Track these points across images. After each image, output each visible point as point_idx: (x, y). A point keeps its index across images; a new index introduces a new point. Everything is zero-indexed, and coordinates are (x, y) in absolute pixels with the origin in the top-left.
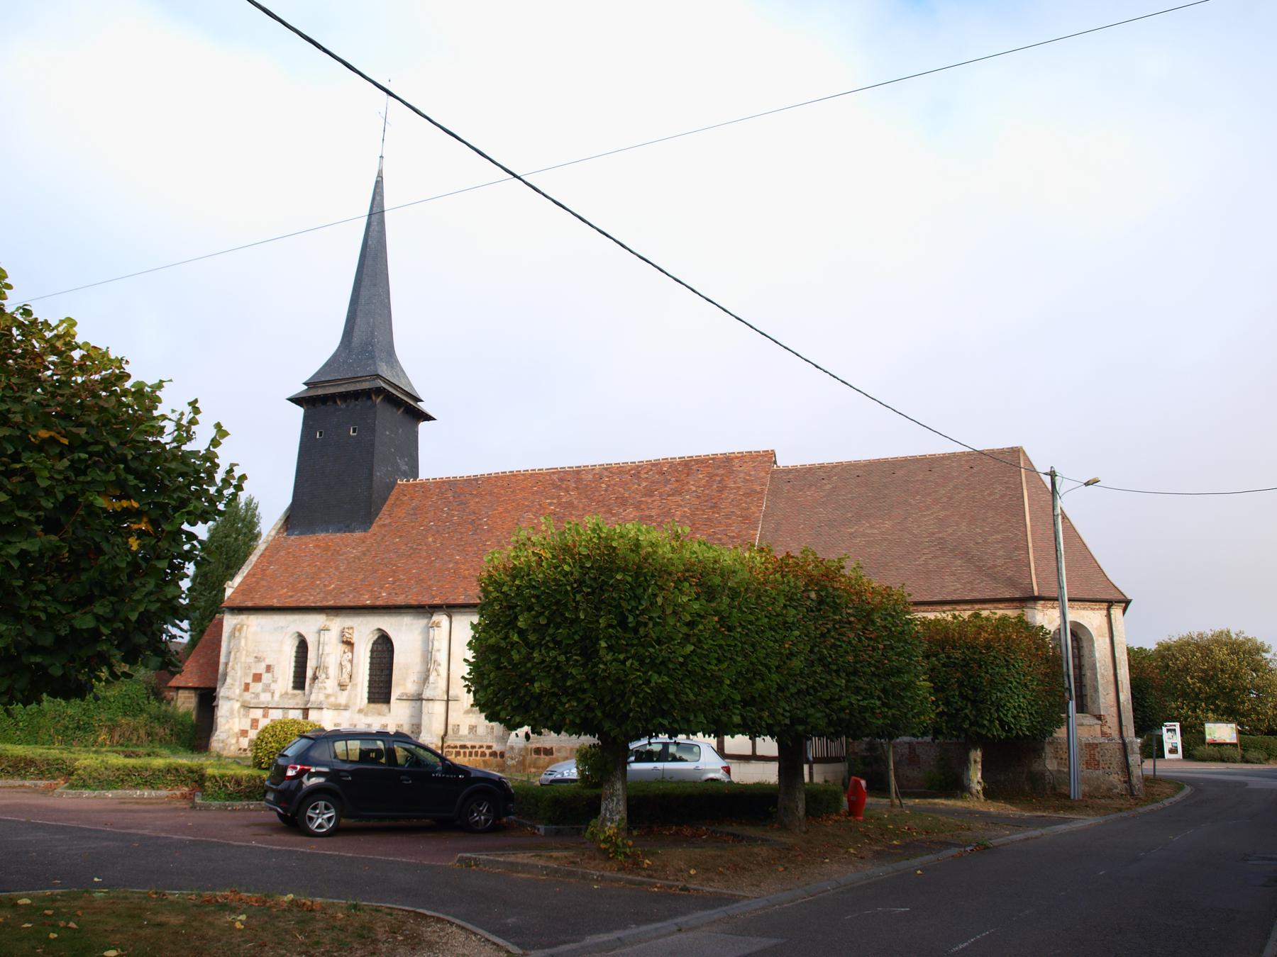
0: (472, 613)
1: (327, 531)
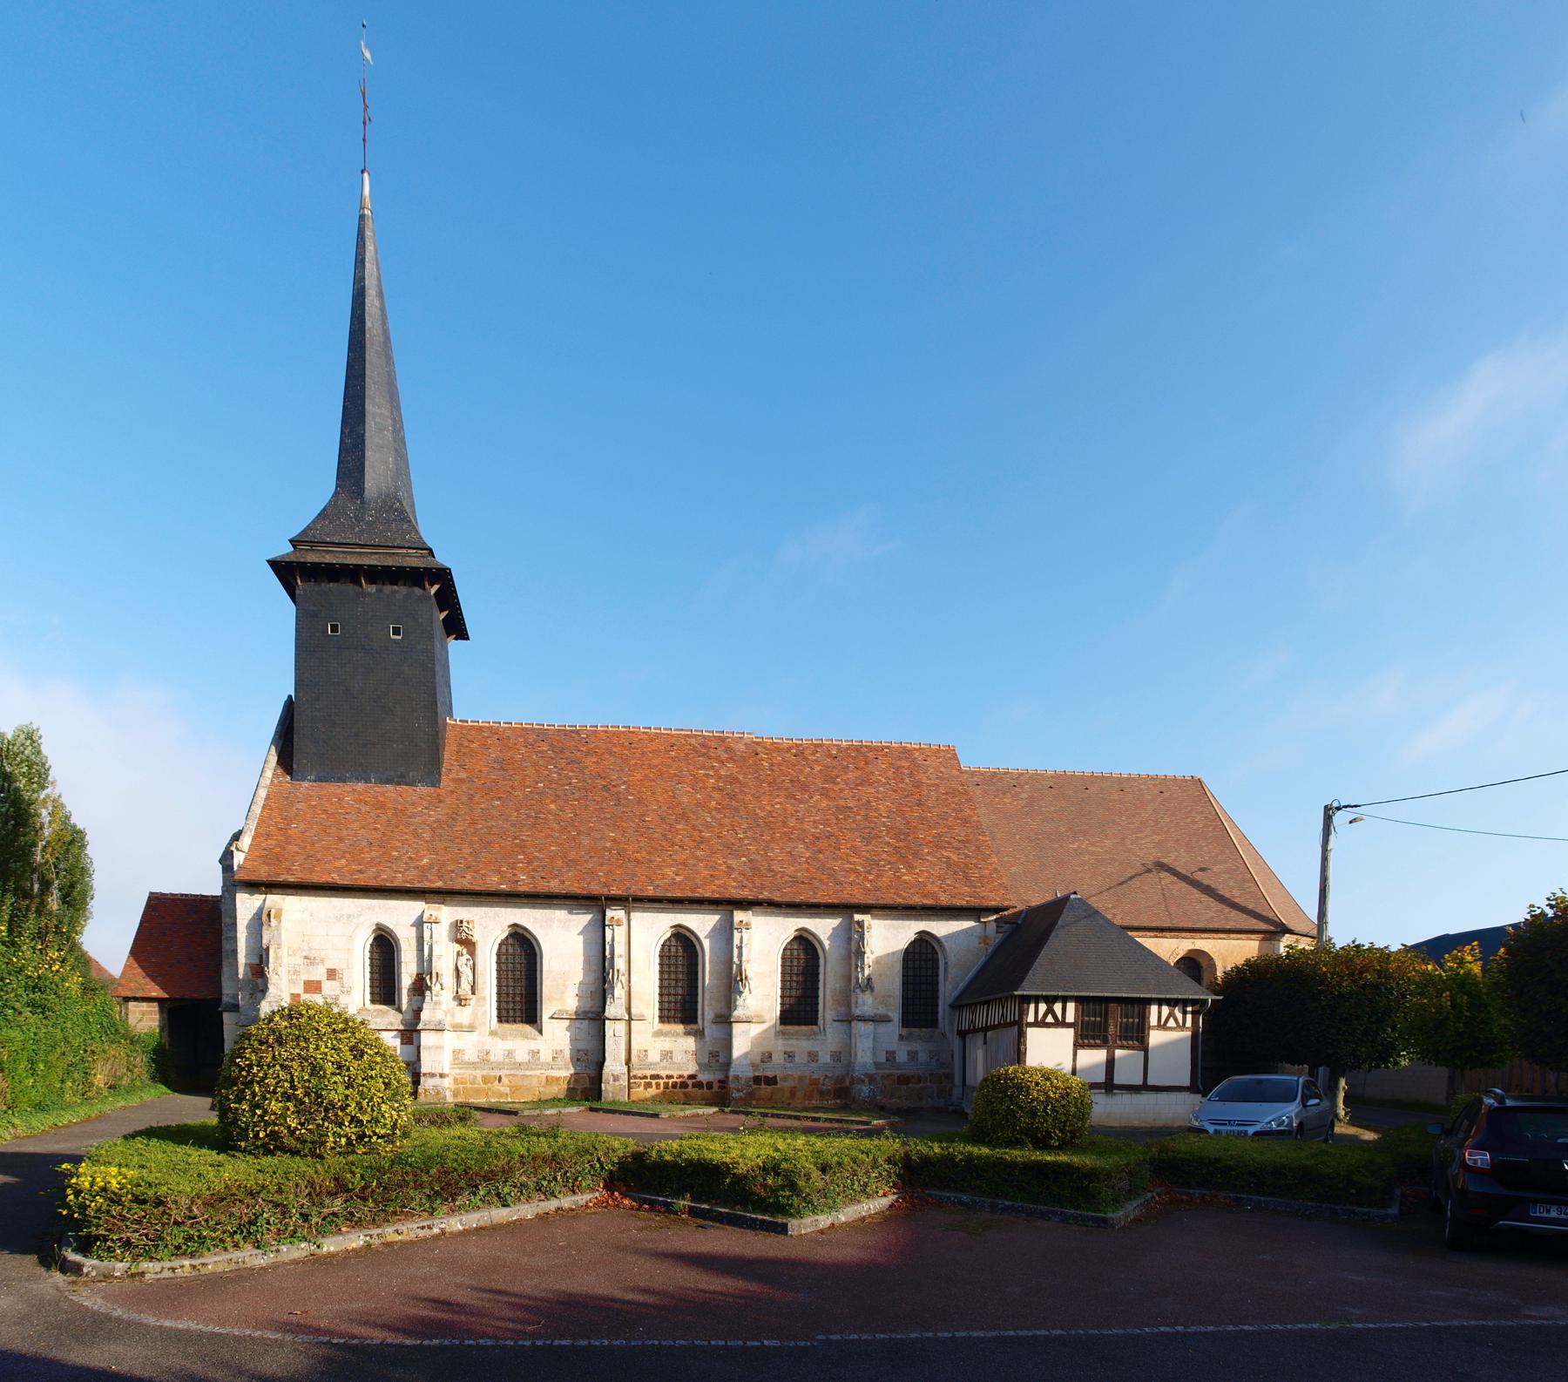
0: (713, 912)
1: (367, 780)
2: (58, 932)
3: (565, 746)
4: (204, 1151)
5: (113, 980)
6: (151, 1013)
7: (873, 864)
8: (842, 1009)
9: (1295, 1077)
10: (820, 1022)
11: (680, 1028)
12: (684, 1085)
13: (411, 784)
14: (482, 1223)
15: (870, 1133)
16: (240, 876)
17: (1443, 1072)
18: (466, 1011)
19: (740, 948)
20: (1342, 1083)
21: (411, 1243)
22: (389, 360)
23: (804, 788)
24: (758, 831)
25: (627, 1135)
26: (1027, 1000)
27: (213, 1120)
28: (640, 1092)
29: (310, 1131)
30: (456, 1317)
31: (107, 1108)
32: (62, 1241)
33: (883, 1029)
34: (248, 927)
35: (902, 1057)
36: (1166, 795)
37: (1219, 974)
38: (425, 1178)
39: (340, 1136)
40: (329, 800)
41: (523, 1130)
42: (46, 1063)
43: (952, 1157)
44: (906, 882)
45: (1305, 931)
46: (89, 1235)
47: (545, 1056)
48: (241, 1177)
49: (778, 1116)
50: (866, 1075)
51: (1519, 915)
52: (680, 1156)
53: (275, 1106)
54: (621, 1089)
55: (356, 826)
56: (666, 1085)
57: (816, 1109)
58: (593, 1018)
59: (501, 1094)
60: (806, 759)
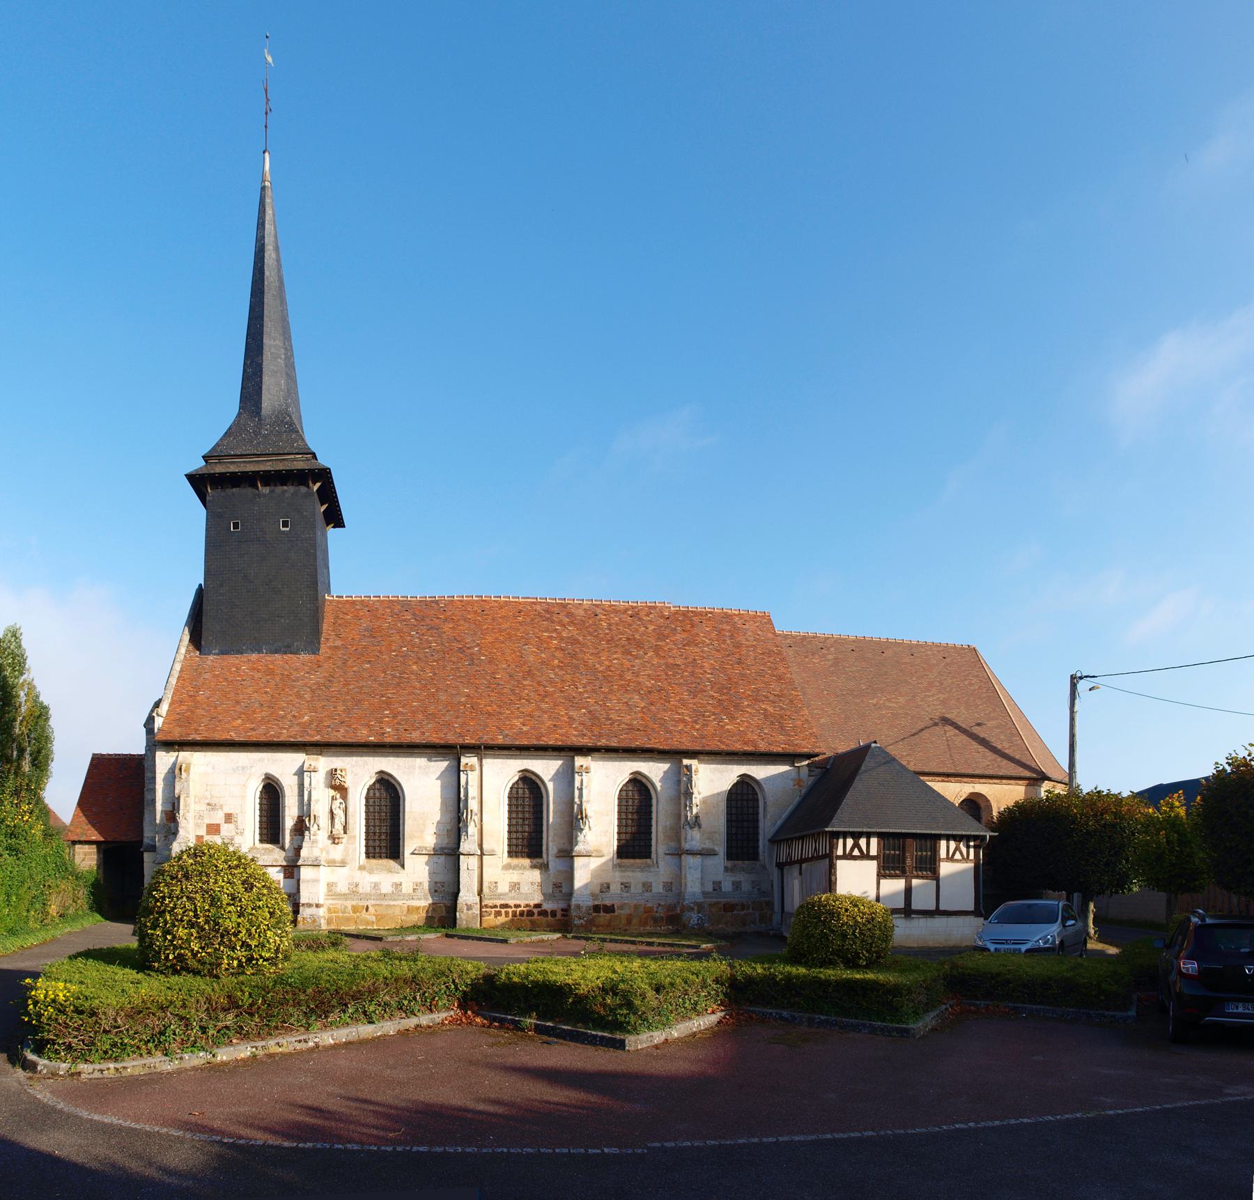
1: (260, 651)
2: (29, 789)
3: (425, 615)
4: (127, 970)
5: (65, 827)
6: (90, 853)
7: (698, 715)
8: (673, 844)
9: (1054, 901)
10: (654, 855)
12: (530, 913)
14: (350, 1038)
15: (699, 956)
16: (159, 737)
17: (1163, 895)
18: (340, 849)
19: (581, 790)
20: (1092, 906)
21: (290, 1054)
22: (283, 301)
23: (639, 645)
24: (597, 683)
25: (479, 959)
26: (836, 835)
27: (134, 944)
28: (491, 920)
29: (209, 954)
30: (327, 1123)
31: (58, 933)
32: (24, 1044)
33: (710, 861)
35: (727, 886)
36: (948, 660)
37: (995, 814)
38: (302, 997)
39: (233, 959)
41: (387, 954)
42: (17, 895)
43: (772, 977)
44: (728, 731)
45: (1060, 778)
46: (42, 1039)
47: (407, 888)
48: (155, 993)
49: (616, 941)
50: (695, 903)
51: (1209, 771)
52: (527, 978)
53: (182, 932)
54: (474, 917)
55: (250, 690)
56: (514, 914)
57: (650, 934)
58: (449, 853)
59: (368, 922)
60: (640, 619)
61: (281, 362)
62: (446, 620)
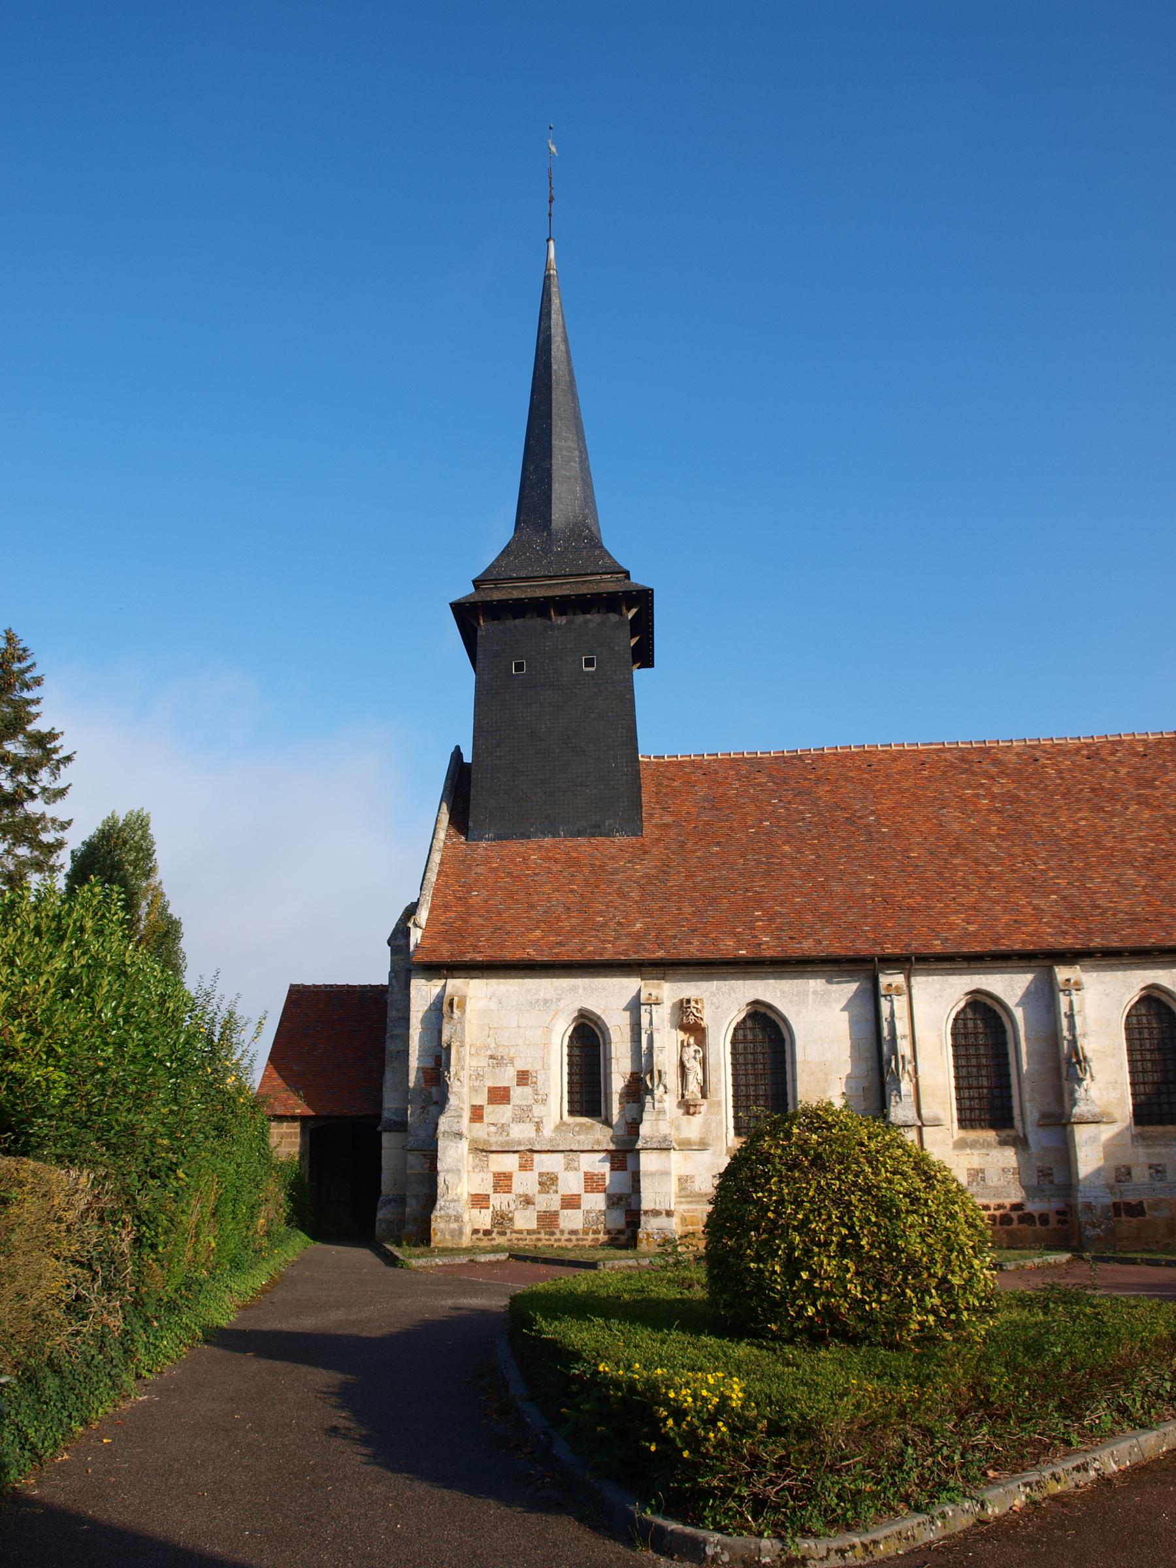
0: (1025, 971)
1: (555, 834)
6: (290, 1135)
11: (990, 1135)
12: (1005, 1220)
13: (608, 834)
16: (419, 958)
19: (1071, 1017)
23: (1113, 797)
24: (1064, 856)
34: (422, 1021)
35: (1141, 1175)
40: (512, 861)
55: (547, 888)
60: (1103, 760)
61: (576, 466)
62: (818, 780)
